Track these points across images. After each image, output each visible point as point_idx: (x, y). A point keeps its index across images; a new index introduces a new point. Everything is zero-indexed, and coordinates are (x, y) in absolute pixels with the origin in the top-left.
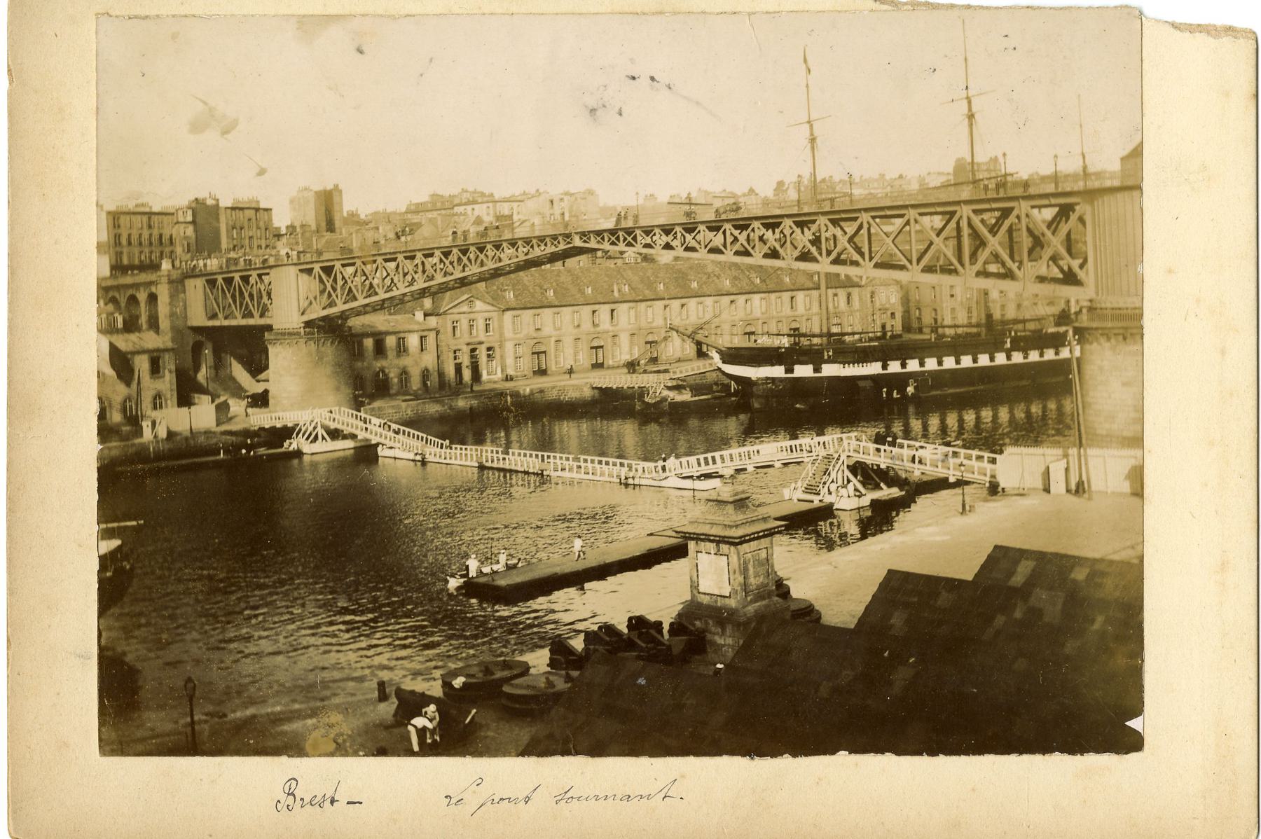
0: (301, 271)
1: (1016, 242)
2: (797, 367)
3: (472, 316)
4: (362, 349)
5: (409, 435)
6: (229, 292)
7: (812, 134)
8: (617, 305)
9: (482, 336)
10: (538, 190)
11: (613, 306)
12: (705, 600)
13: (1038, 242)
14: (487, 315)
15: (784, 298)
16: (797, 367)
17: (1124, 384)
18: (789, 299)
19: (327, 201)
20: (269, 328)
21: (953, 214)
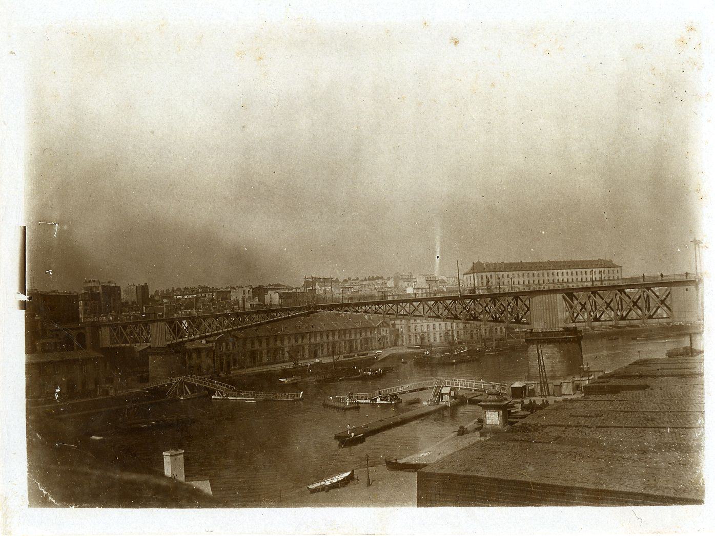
19: (144, 289)
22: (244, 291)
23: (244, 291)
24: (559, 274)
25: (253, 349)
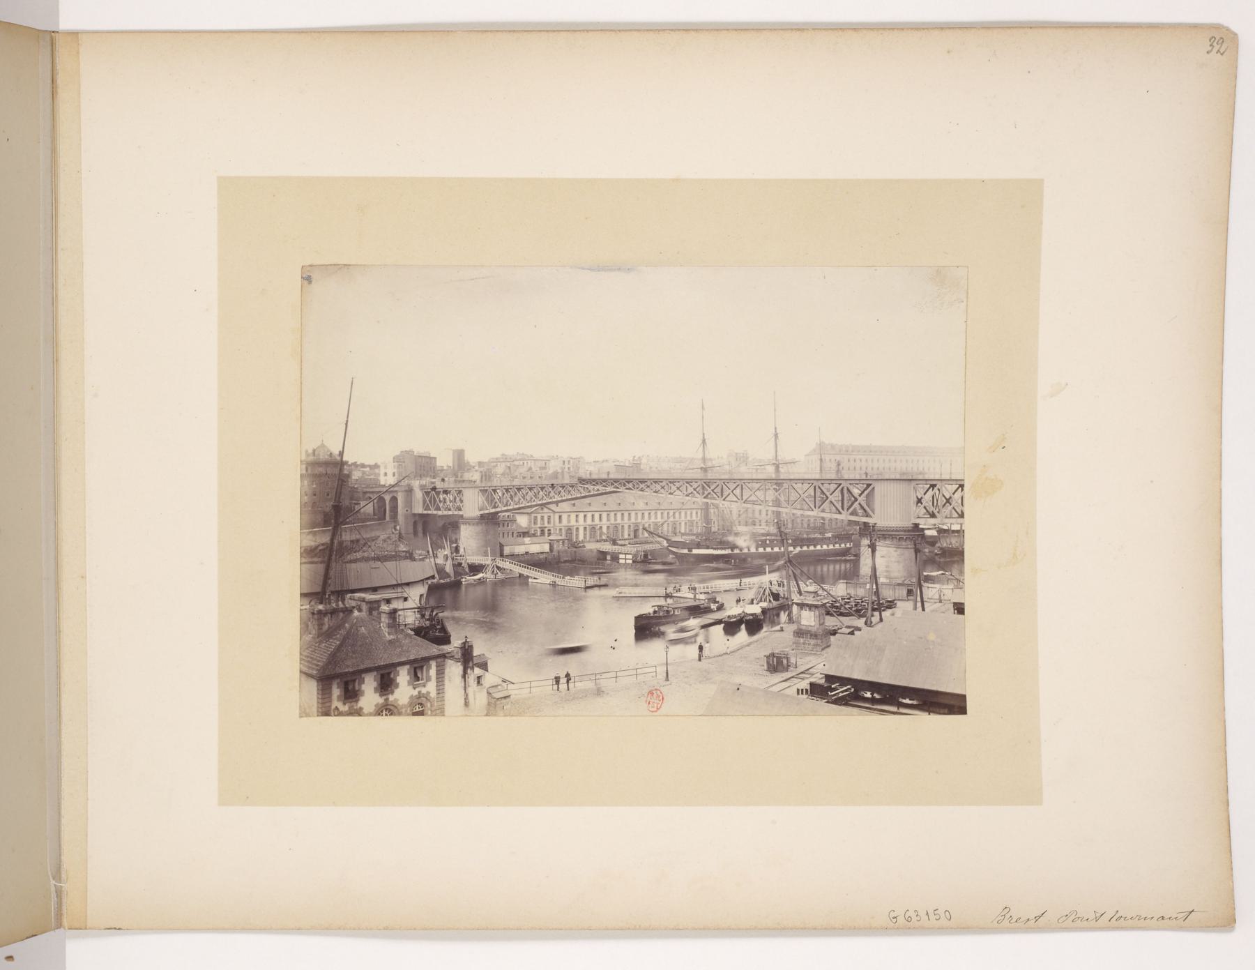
3: (543, 515)
14: (549, 514)
19: (459, 454)
22: (564, 462)
23: (564, 462)
24: (851, 460)
25: (593, 523)
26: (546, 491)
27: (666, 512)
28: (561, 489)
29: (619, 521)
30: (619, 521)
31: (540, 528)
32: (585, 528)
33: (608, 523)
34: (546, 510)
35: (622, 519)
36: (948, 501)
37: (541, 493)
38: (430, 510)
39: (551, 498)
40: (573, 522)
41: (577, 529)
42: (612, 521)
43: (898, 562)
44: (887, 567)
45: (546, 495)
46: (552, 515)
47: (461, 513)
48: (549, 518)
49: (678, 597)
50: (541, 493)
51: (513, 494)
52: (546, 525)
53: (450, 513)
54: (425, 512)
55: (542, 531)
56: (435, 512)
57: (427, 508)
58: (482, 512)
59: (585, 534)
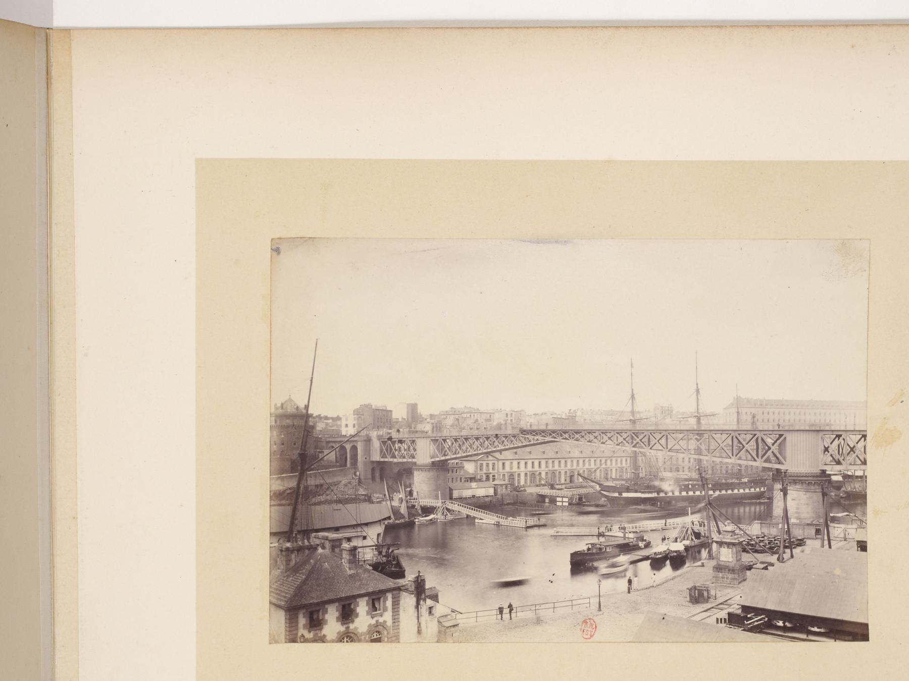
0: (432, 440)
1: (531, 426)
2: (623, 494)
4: (298, 481)
5: (497, 517)
6: (384, 447)
7: (632, 393)
8: (520, 460)
9: (491, 471)
10: (501, 409)
11: (519, 461)
12: (722, 563)
13: (852, 449)
14: (493, 462)
15: (574, 461)
16: (623, 494)
17: (793, 500)
18: (564, 462)
19: (413, 408)
20: (415, 463)
21: (755, 435)
22: (507, 414)
23: (507, 414)
25: (533, 470)
26: (490, 441)
27: (599, 459)
28: (504, 439)
29: (556, 467)
30: (556, 467)
31: (485, 474)
32: (526, 474)
33: (547, 469)
34: (490, 458)
35: (560, 466)
36: (852, 449)
37: (486, 442)
38: (386, 457)
39: (495, 447)
40: (515, 469)
41: (519, 475)
42: (551, 468)
43: (807, 504)
44: (797, 508)
45: (491, 444)
46: (496, 462)
47: (414, 460)
48: (494, 465)
49: (612, 536)
50: (486, 442)
51: (461, 444)
52: (491, 471)
53: (405, 460)
54: (382, 460)
55: (487, 476)
56: (391, 460)
57: (384, 456)
58: (433, 460)
59: (526, 480)
